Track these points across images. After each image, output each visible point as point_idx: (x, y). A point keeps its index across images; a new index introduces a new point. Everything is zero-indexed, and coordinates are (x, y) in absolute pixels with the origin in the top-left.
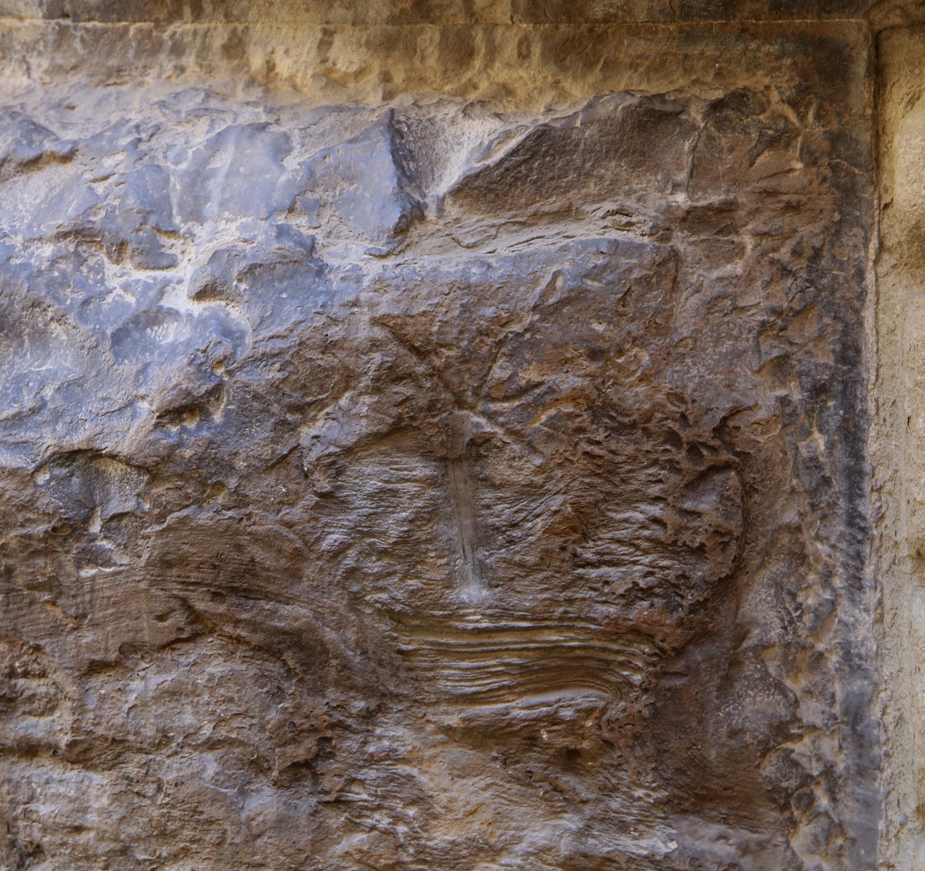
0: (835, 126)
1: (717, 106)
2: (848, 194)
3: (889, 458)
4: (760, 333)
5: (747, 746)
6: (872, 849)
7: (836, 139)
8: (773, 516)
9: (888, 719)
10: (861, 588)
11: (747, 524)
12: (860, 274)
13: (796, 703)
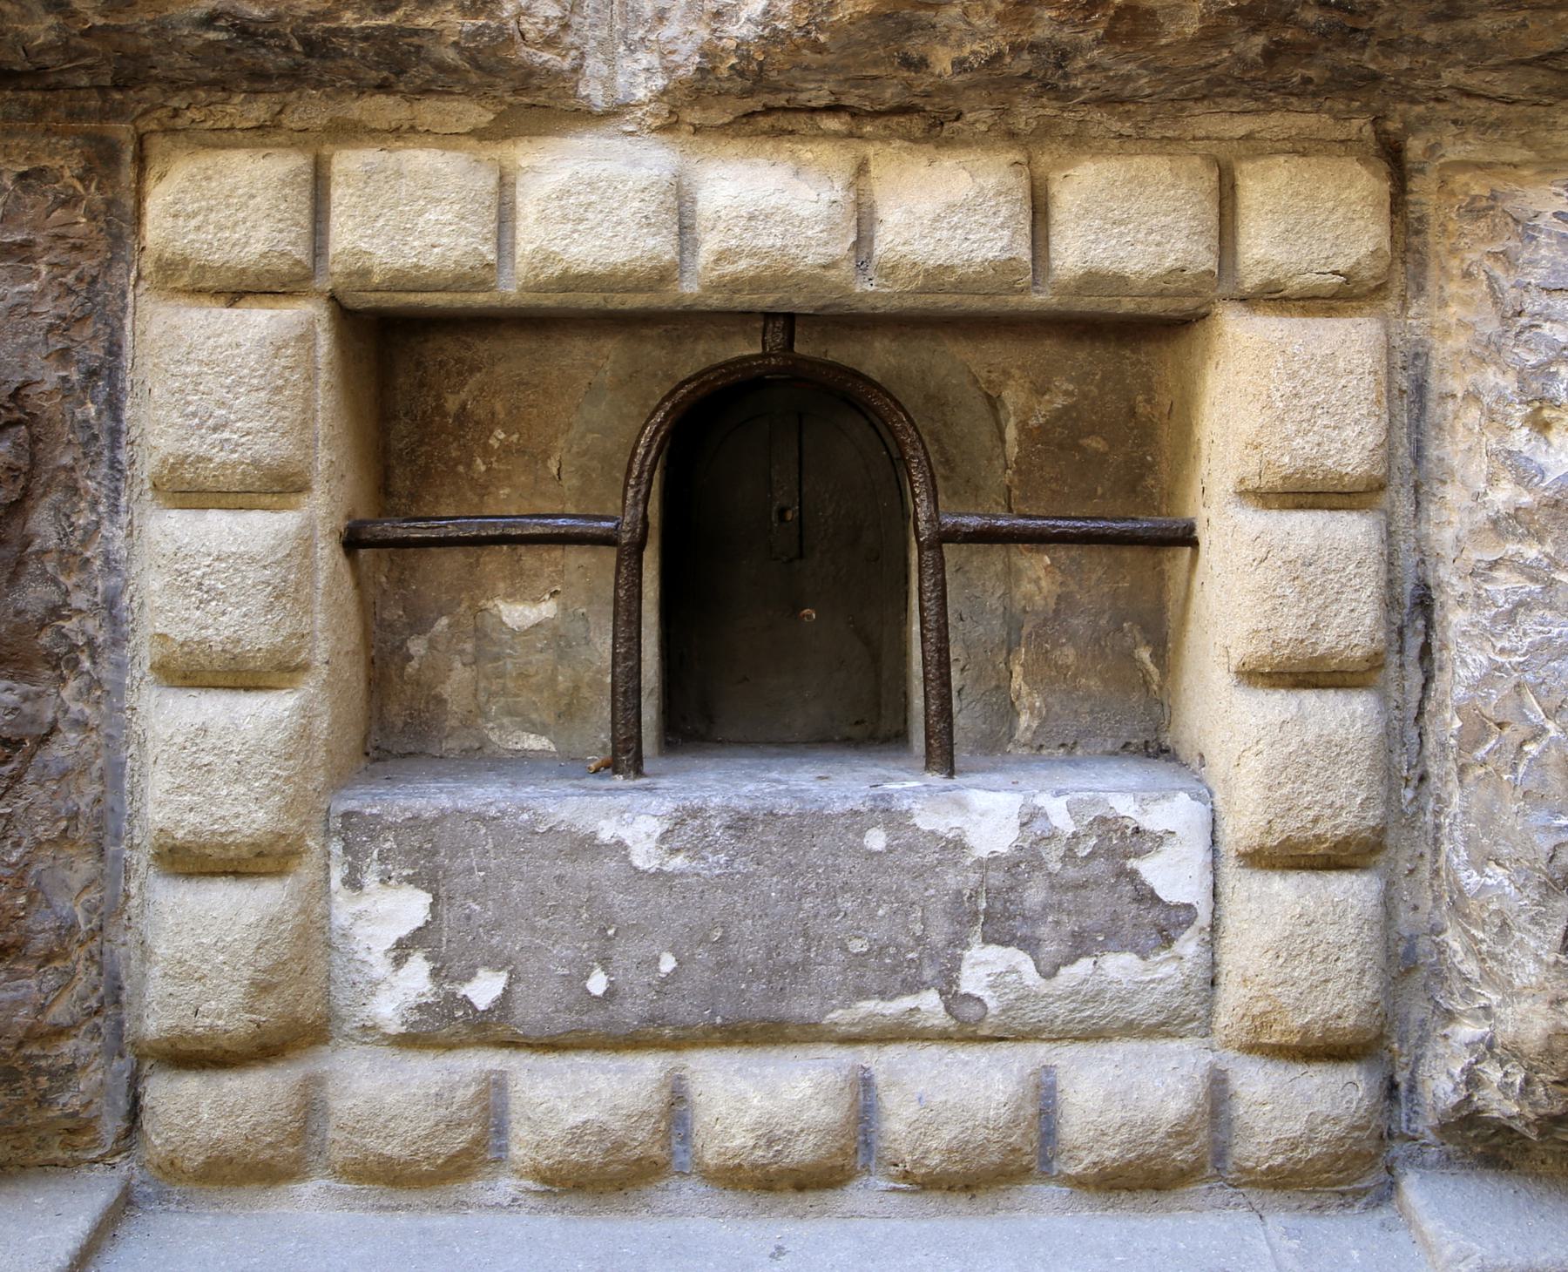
0: (110, 195)
1: (22, 176)
2: (117, 240)
3: (139, 420)
4: (48, 331)
5: (28, 622)
6: (121, 698)
7: (110, 203)
8: (53, 459)
9: (134, 605)
10: (117, 513)
11: (34, 463)
12: (124, 295)
13: (67, 593)
